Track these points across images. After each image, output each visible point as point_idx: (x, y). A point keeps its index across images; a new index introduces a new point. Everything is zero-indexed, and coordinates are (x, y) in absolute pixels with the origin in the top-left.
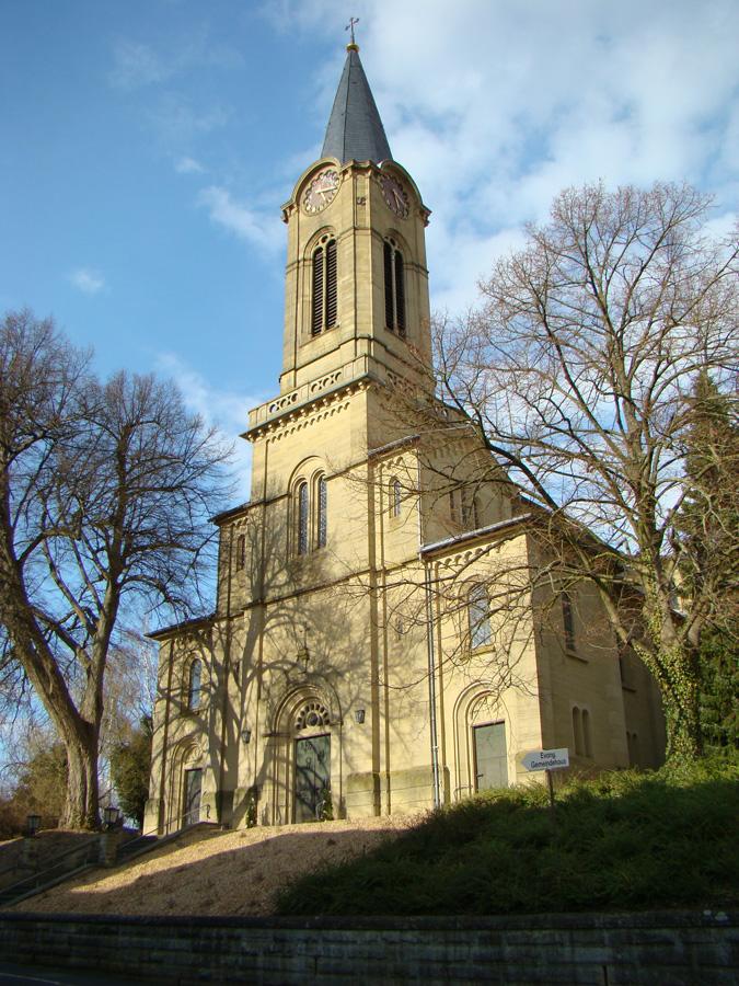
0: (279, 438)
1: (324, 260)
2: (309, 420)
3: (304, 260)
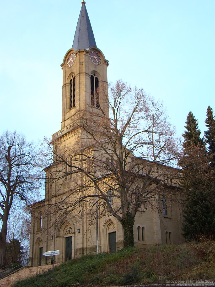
0: (68, 139)
1: (73, 83)
2: (67, 138)
3: (67, 83)
